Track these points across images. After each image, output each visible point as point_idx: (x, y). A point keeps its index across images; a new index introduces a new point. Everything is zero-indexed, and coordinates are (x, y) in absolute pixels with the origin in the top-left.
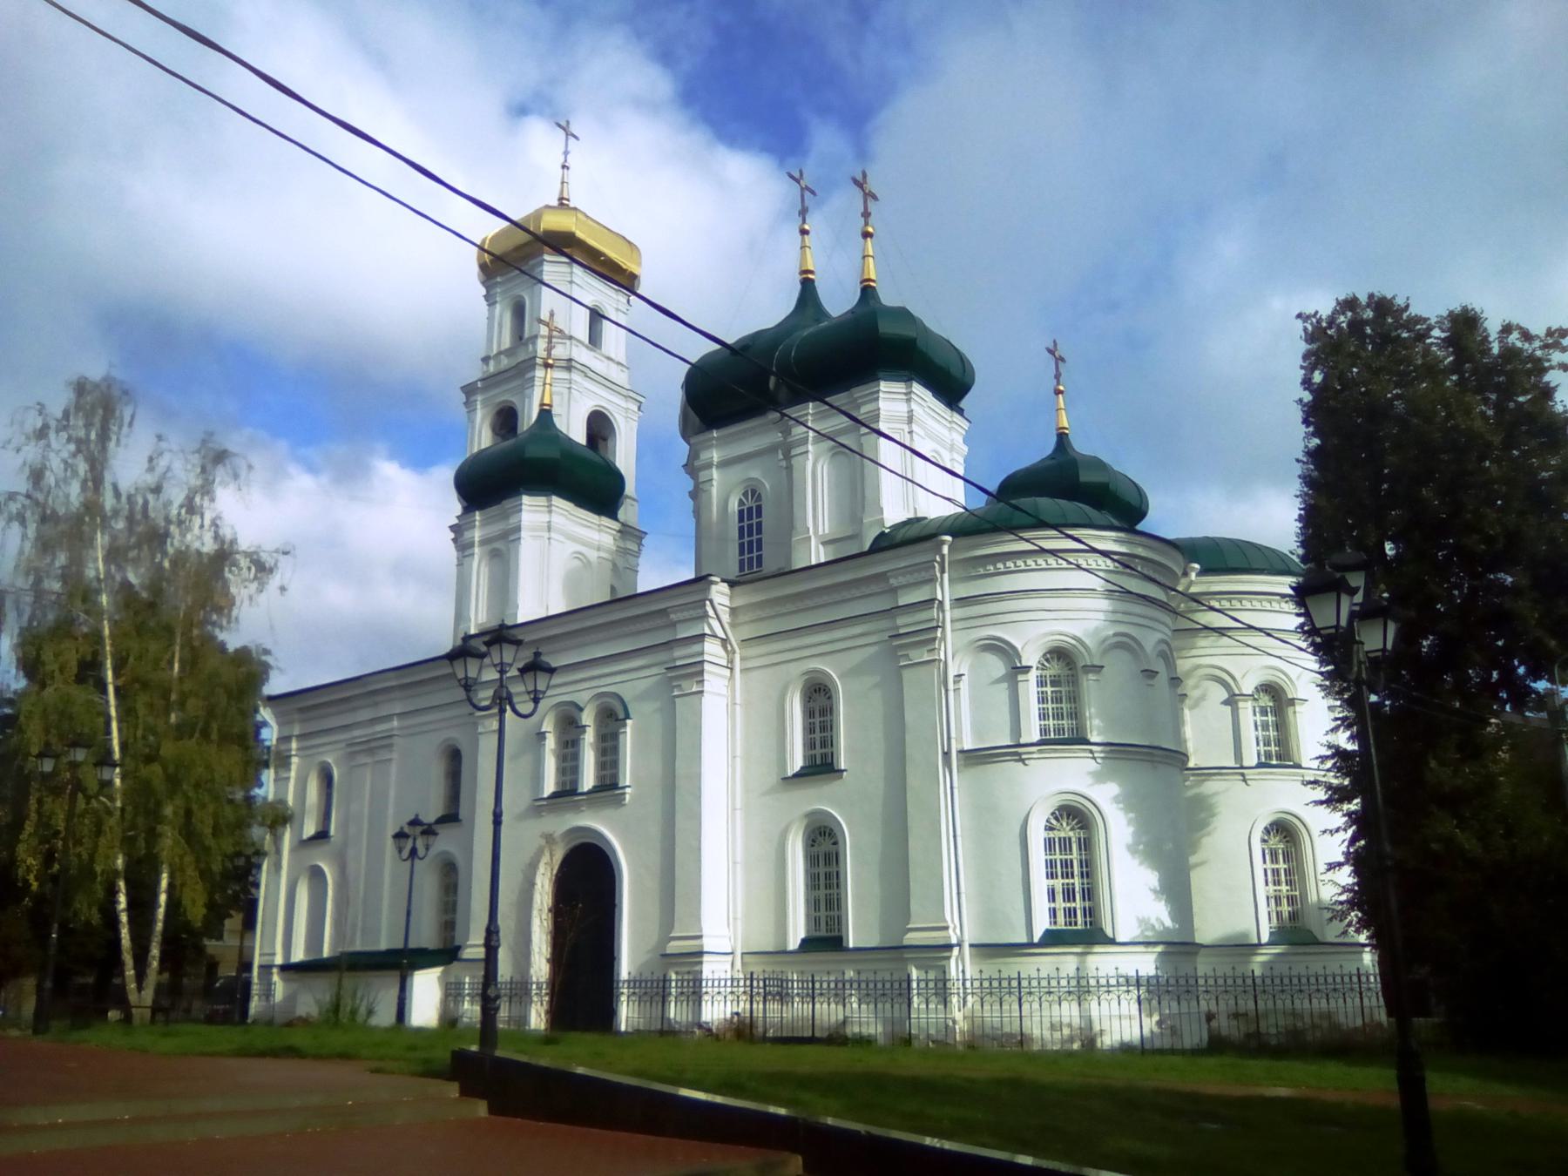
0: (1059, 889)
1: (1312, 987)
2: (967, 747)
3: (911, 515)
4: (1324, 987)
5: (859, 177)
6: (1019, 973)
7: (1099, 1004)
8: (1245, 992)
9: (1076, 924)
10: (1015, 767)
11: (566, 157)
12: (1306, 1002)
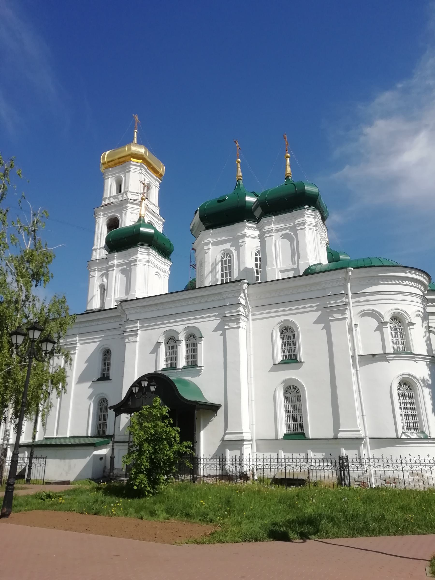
0: (291, 416)
1: (217, 463)
2: (362, 353)
3: (319, 262)
4: (314, 464)
7: (431, 473)
8: (397, 466)
9: (298, 431)
10: (384, 363)
12: (391, 472)
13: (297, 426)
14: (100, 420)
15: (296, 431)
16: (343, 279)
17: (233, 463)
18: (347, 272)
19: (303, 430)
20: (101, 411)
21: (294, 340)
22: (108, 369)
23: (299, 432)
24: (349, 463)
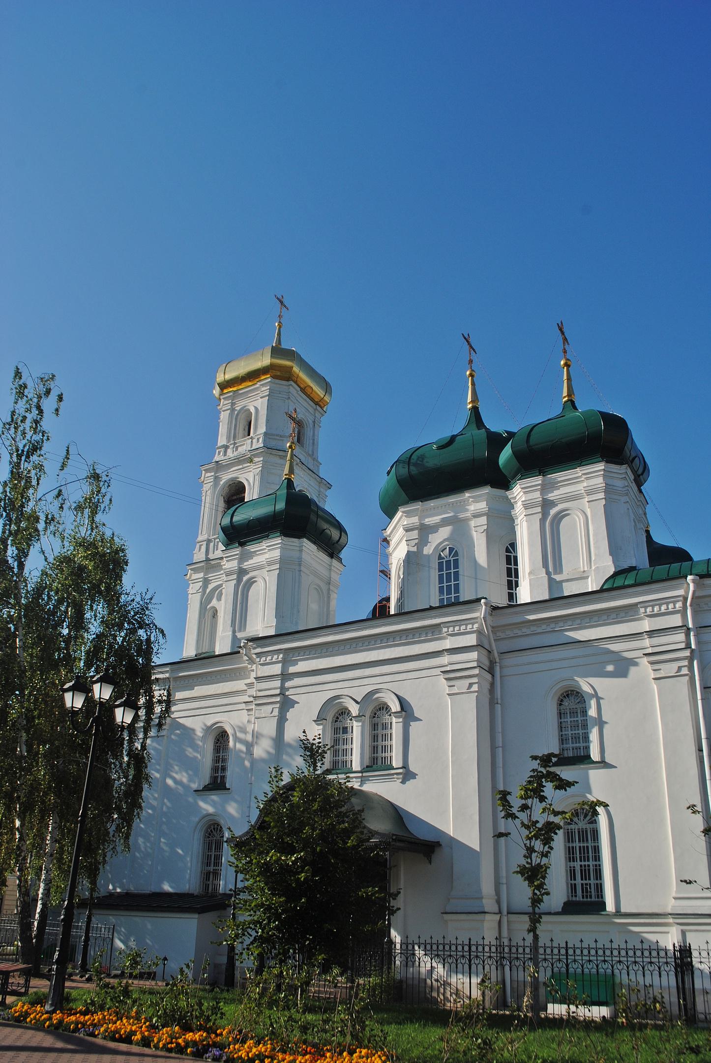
1: (661, 960)
4: (657, 960)
7: (644, 976)
8: (701, 962)
9: (591, 897)
13: (590, 889)
14: (208, 864)
15: (587, 898)
17: (465, 954)
20: (210, 849)
22: (224, 769)
23: (593, 899)
24: (693, 959)
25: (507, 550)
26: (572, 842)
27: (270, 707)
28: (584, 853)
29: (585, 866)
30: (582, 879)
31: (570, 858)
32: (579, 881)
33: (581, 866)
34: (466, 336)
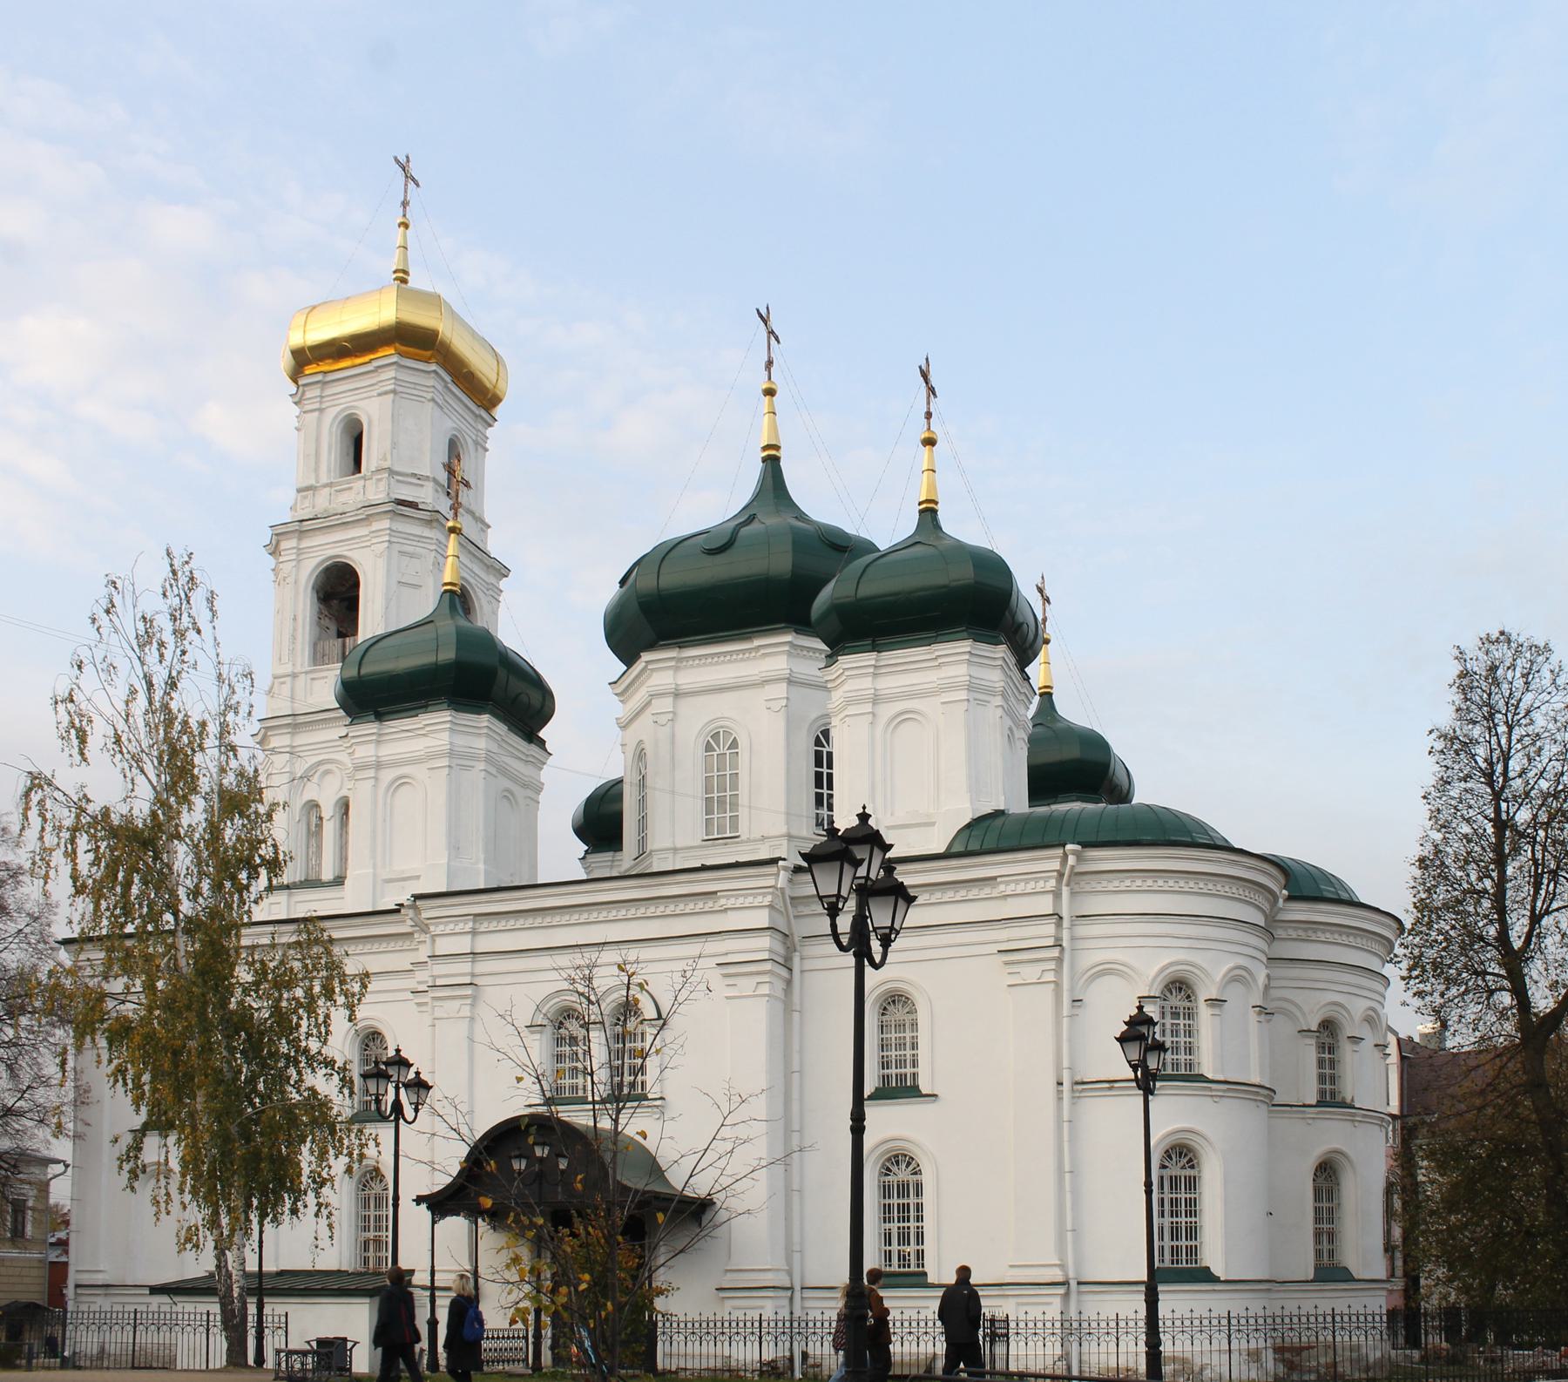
5: (403, 160)
6: (1333, 1309)
8: (1108, 1333)
9: (909, 1266)
11: (405, 211)
14: (366, 1229)
16: (1055, 874)
18: (1065, 857)
19: (923, 1266)
21: (920, 1224)
25: (818, 742)
26: (889, 1198)
27: (457, 1003)
28: (904, 1212)
29: (904, 1228)
30: (899, 1245)
31: (885, 1218)
32: (895, 1247)
33: (899, 1228)
34: (764, 313)
